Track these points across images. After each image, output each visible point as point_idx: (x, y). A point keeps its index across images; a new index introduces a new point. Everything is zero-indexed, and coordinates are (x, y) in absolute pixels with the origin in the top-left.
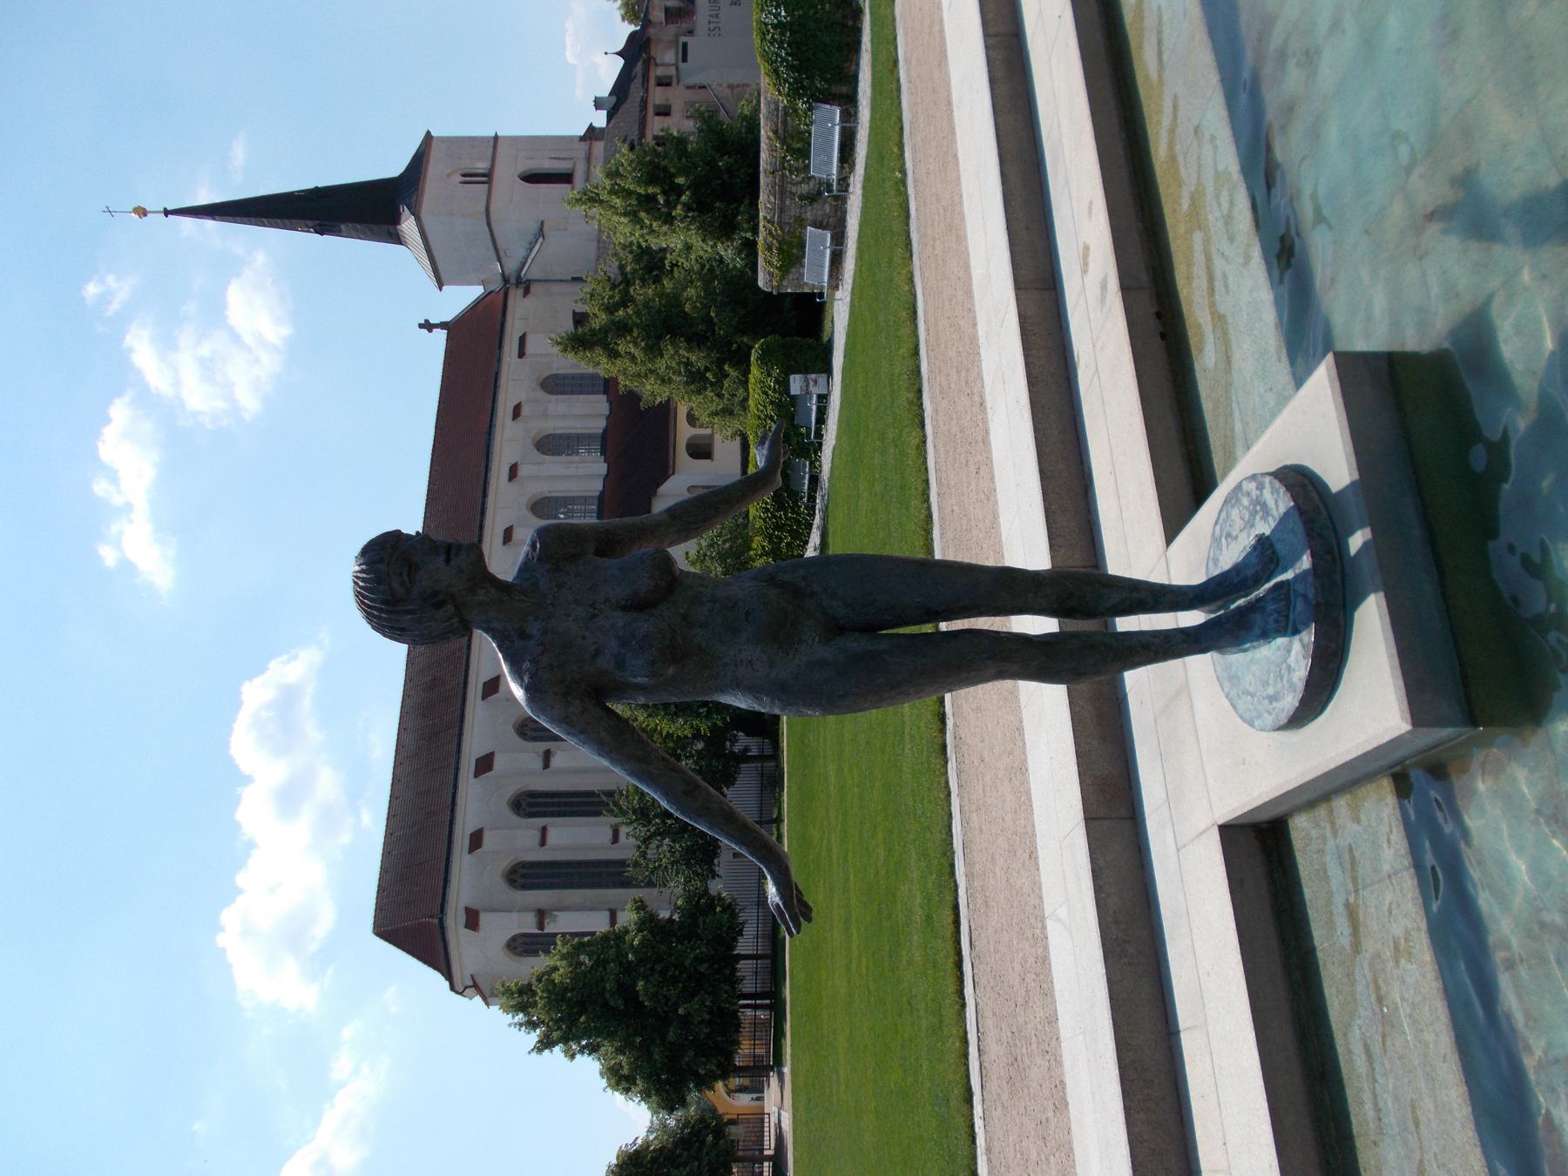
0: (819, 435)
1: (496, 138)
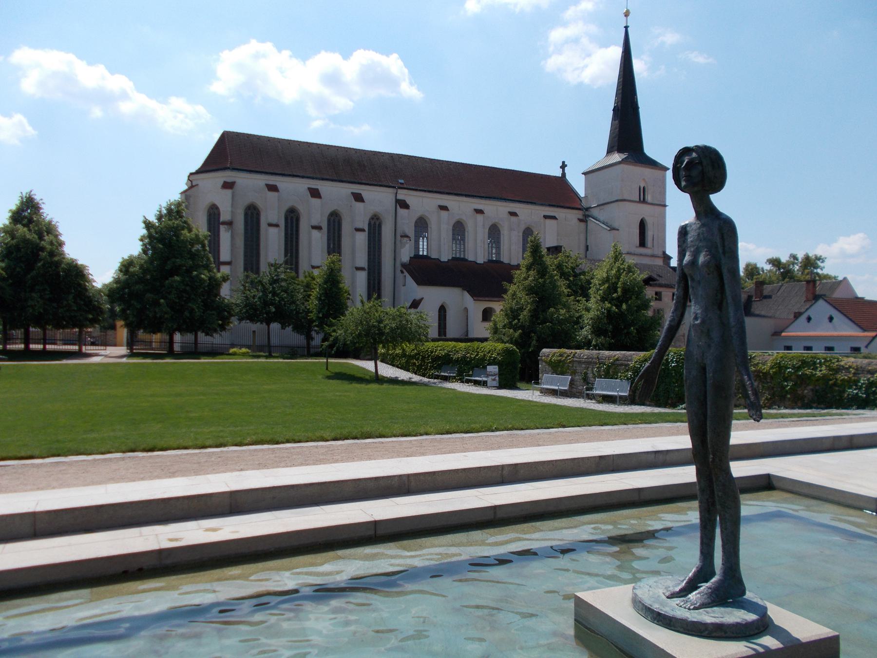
0: (468, 381)
1: (665, 206)
